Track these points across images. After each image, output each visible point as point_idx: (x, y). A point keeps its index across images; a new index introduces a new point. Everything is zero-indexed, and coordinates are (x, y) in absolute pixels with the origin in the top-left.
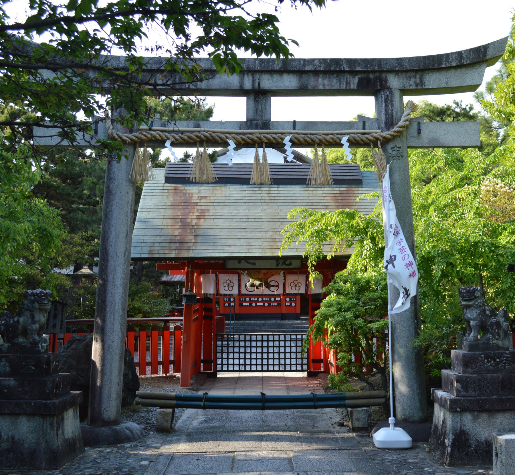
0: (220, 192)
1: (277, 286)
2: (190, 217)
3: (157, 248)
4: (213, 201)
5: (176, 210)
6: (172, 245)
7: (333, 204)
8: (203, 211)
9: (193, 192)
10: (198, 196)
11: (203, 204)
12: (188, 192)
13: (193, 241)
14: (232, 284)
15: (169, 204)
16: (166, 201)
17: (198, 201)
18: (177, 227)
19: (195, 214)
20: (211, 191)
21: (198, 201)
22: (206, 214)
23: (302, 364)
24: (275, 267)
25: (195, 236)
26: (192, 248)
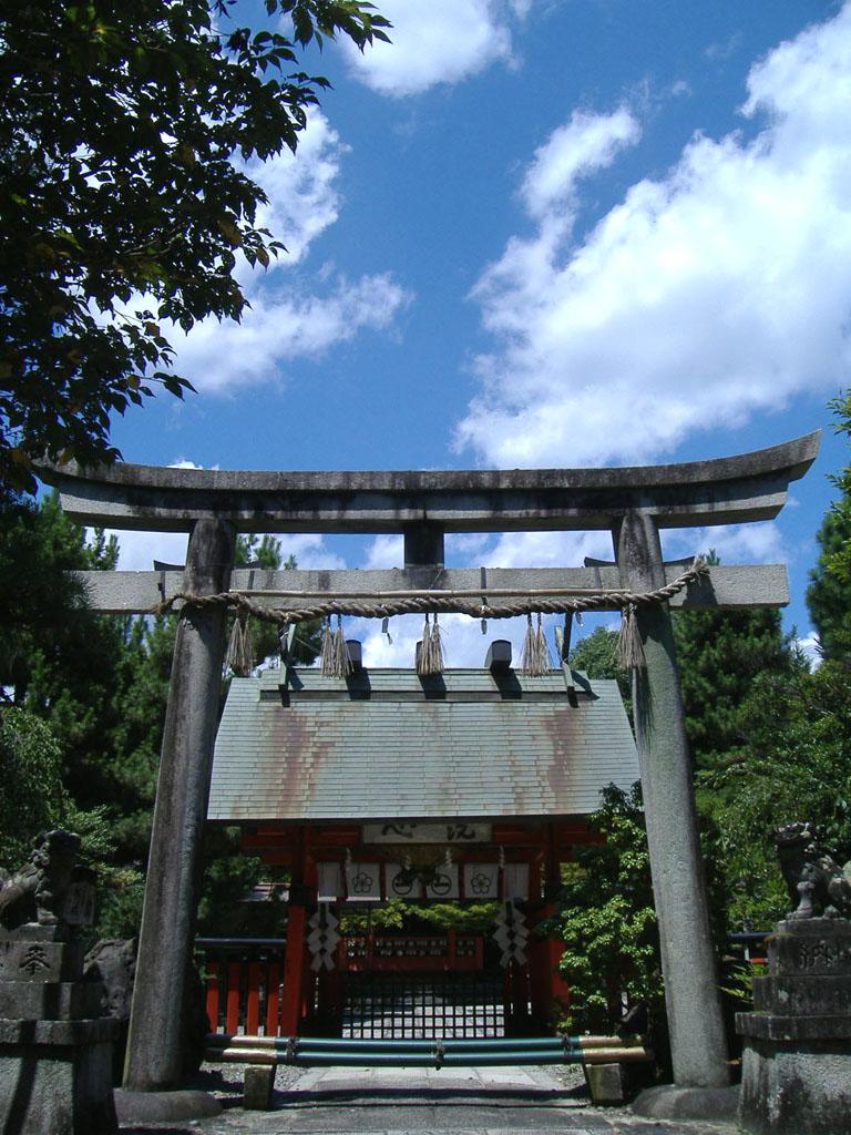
0: (352, 714)
1: (447, 885)
2: (303, 755)
3: (245, 804)
4: (340, 729)
5: (280, 744)
6: (271, 799)
7: (545, 733)
8: (324, 745)
9: (308, 714)
10: (316, 722)
11: (324, 735)
12: (298, 714)
13: (307, 793)
14: (369, 881)
15: (267, 734)
16: (262, 728)
17: (316, 729)
18: (281, 771)
19: (310, 750)
20: (338, 714)
21: (316, 729)
22: (329, 750)
23: (495, 1027)
24: (447, 841)
25: (310, 785)
26: (304, 804)
